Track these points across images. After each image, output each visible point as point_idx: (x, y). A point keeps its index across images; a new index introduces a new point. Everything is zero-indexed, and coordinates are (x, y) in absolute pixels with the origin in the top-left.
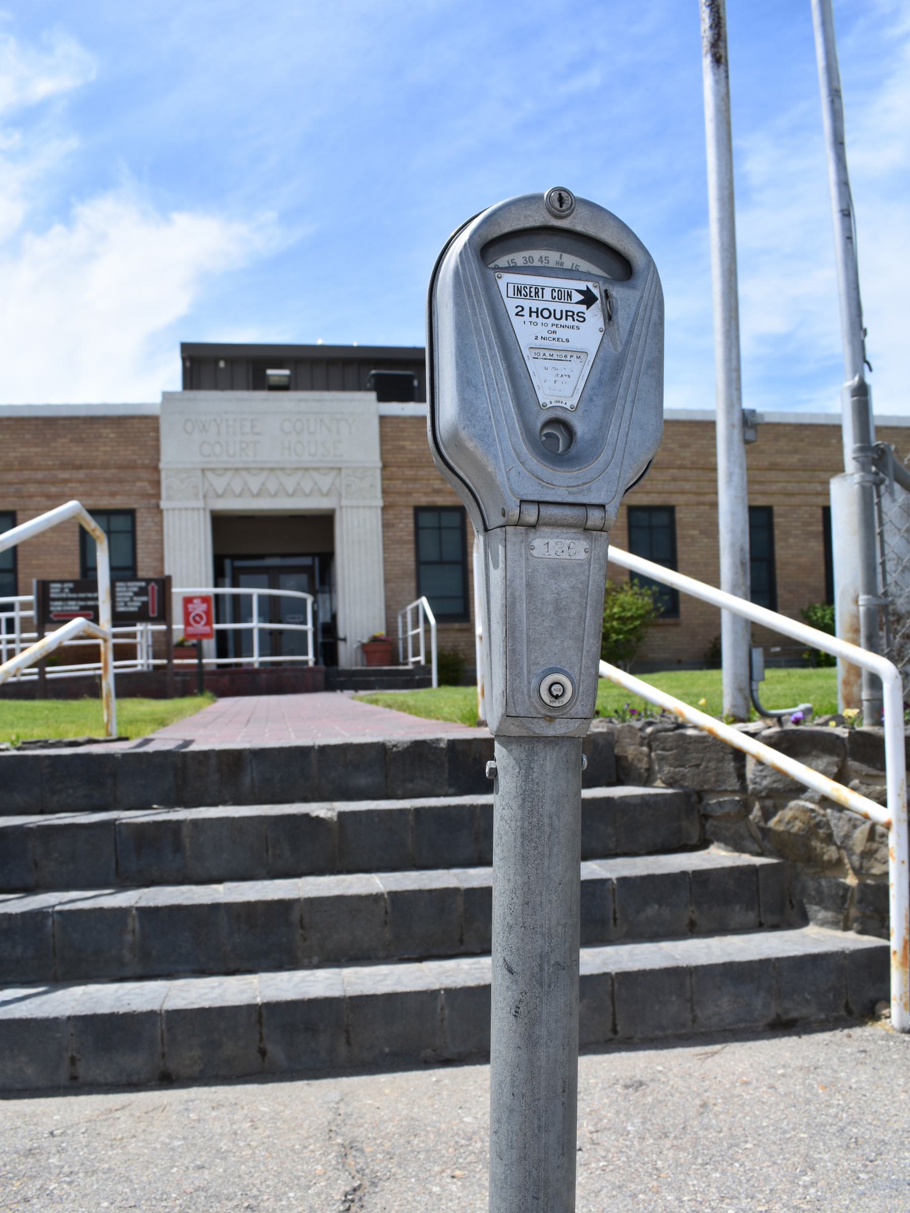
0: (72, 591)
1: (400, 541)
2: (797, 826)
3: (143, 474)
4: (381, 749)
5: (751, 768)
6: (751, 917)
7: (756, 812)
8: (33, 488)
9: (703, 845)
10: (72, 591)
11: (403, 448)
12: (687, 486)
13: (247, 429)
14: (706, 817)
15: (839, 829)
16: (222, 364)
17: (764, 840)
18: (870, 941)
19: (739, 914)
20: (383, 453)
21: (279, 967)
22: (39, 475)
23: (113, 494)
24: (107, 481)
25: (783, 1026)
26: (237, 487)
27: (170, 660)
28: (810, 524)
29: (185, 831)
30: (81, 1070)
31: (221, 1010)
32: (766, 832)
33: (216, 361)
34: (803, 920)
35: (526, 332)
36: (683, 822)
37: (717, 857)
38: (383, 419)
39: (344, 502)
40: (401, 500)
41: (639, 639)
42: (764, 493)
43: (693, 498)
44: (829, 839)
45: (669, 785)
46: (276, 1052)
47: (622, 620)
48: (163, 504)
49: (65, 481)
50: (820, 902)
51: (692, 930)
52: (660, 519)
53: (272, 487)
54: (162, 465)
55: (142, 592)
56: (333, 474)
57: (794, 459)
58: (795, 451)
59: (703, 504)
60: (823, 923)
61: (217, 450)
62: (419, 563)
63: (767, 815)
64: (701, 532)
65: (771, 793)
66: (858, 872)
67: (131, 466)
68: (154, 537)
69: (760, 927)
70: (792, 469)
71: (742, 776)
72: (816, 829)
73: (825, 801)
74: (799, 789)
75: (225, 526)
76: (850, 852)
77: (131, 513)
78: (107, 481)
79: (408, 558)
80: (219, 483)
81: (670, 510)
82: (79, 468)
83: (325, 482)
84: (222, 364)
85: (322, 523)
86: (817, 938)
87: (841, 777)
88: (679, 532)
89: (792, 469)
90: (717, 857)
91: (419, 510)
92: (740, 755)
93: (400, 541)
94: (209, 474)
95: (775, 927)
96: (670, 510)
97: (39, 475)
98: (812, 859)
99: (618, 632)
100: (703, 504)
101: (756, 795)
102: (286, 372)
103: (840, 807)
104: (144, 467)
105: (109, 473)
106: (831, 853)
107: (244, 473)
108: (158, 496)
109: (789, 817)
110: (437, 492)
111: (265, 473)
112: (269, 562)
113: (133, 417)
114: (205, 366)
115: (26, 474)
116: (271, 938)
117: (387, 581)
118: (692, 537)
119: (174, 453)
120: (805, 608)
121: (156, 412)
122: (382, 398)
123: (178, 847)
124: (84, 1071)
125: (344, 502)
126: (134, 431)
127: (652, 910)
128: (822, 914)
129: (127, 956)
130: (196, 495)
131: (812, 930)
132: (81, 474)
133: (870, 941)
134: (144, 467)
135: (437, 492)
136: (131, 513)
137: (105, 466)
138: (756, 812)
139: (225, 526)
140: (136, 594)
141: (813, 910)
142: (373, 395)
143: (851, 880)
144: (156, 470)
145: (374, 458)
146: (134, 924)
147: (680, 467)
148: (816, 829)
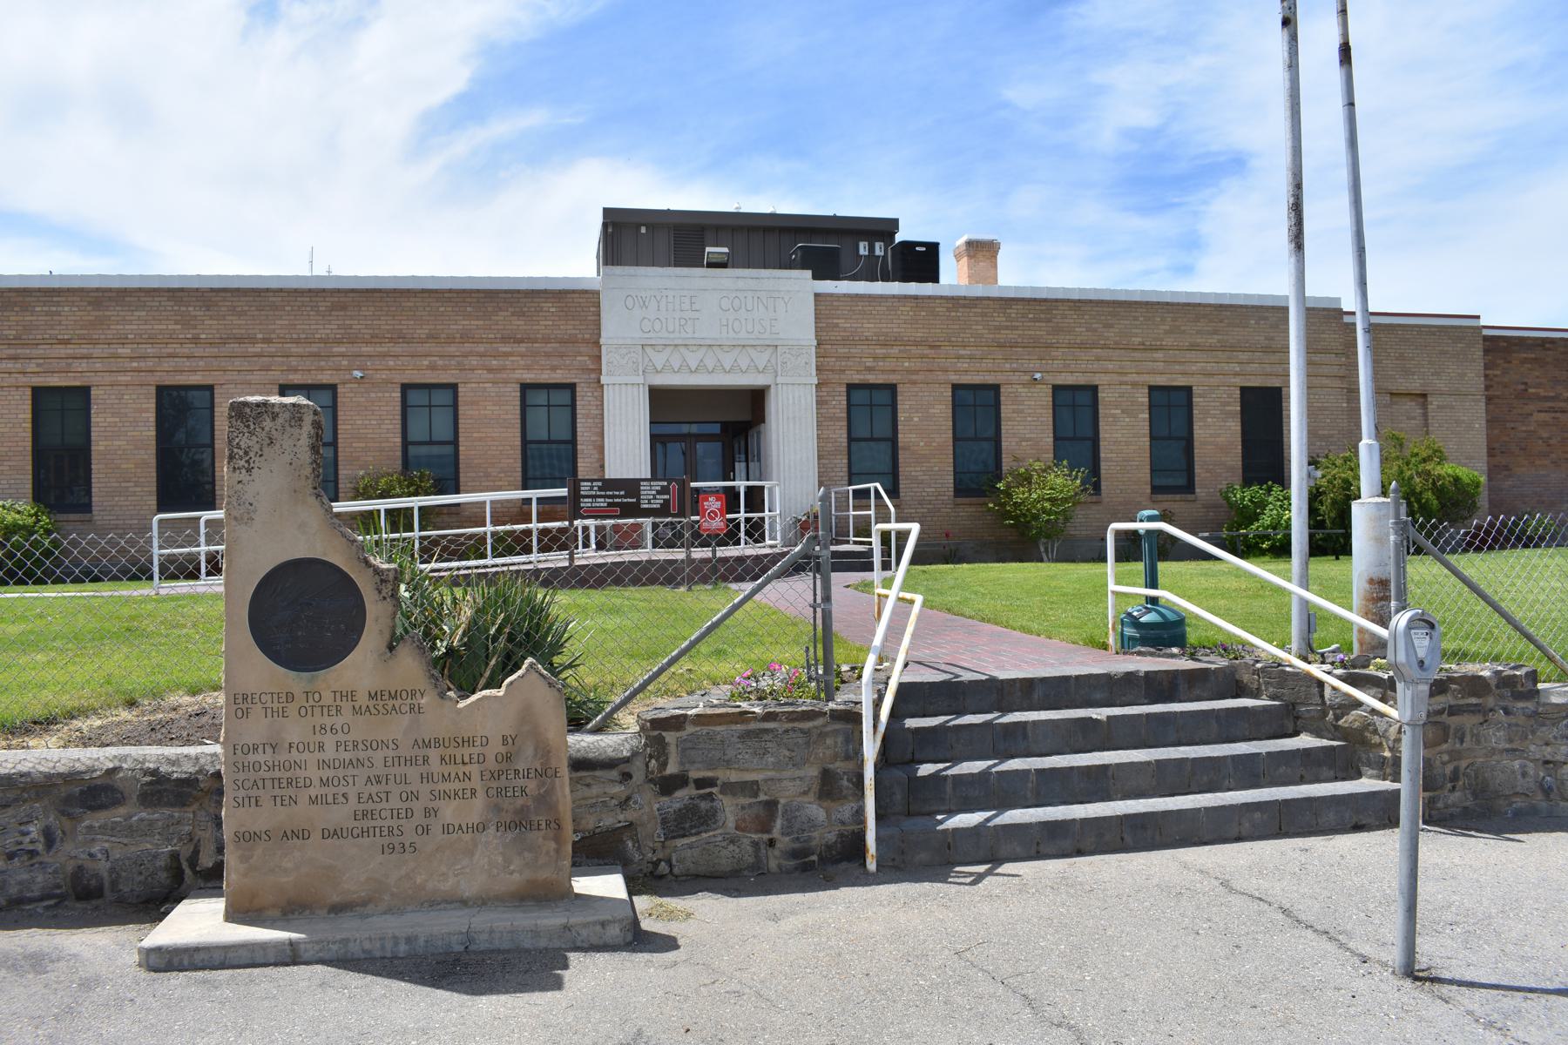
0: (600, 489)
1: (833, 418)
2: (1357, 724)
3: (583, 348)
4: (1108, 677)
5: (1328, 692)
6: (1332, 773)
7: (1331, 715)
8: (474, 361)
9: (1296, 734)
10: (600, 489)
11: (837, 325)
12: (1110, 366)
13: (686, 306)
14: (1297, 718)
15: (1381, 724)
16: (643, 230)
17: (1336, 732)
18: (1387, 785)
19: (1326, 772)
20: (818, 330)
21: (1103, 800)
22: (481, 348)
23: (554, 368)
24: (548, 355)
25: (1358, 828)
26: (676, 362)
27: (688, 556)
28: (1228, 404)
29: (1029, 727)
30: (1041, 848)
31: (1104, 818)
32: (1337, 728)
33: (638, 226)
34: (1359, 775)
35: (1416, 642)
36: (1285, 721)
37: (1305, 741)
38: (817, 295)
39: (779, 380)
40: (834, 377)
41: (1067, 519)
42: (1184, 374)
43: (1115, 378)
44: (1375, 732)
45: (1272, 698)
46: (1128, 839)
47: (1052, 500)
48: (604, 380)
49: (507, 355)
50: (1369, 765)
51: (1302, 780)
52: (1083, 399)
53: (710, 364)
54: (602, 341)
55: (664, 490)
56: (770, 350)
57: (1214, 340)
58: (1215, 332)
59: (1126, 383)
60: (1371, 777)
61: (657, 326)
62: (851, 439)
63: (1337, 718)
64: (1123, 412)
65: (1340, 706)
66: (1391, 749)
67: (572, 341)
68: (595, 412)
69: (1336, 779)
70: (1211, 349)
71: (1322, 696)
72: (1367, 726)
73: (1374, 711)
74: (1358, 704)
75: (663, 401)
76: (1387, 739)
77: (572, 387)
78: (548, 355)
79: (842, 436)
80: (659, 359)
81: (1094, 389)
82: (521, 341)
83: (762, 359)
84: (643, 230)
85: (756, 399)
86: (1366, 784)
87: (1383, 700)
88: (1101, 411)
89: (1211, 349)
90: (1305, 741)
91: (851, 387)
92: (1321, 684)
93: (833, 418)
94: (648, 350)
95: (1344, 779)
96: (1094, 389)
97: (481, 348)
98: (1365, 742)
99: (1049, 513)
100: (1126, 383)
101: (1332, 707)
102: (726, 250)
103: (1382, 715)
104: (585, 341)
105: (549, 347)
106: (1376, 739)
107: (682, 349)
108: (600, 371)
109: (1351, 719)
110: (870, 369)
111: (703, 350)
112: (685, 429)
113: (574, 292)
114: (629, 236)
115: (468, 347)
116: (1098, 784)
117: (819, 457)
118: (1114, 416)
119: (615, 328)
120: (1224, 487)
121: (596, 287)
122: (815, 277)
123: (1025, 737)
124: (1043, 849)
125: (779, 380)
126: (570, 307)
127: (1282, 770)
128: (1370, 772)
129: (1029, 794)
130: (636, 370)
131: (1364, 780)
132: (522, 348)
133: (1387, 785)
134: (585, 341)
135: (870, 369)
136: (572, 387)
137: (546, 340)
138: (1331, 715)
139: (663, 401)
140: (658, 492)
141: (1364, 769)
142: (809, 273)
143: (1387, 754)
144: (597, 344)
145: (808, 336)
146: (1033, 778)
147: (1105, 347)
148: (1367, 726)
